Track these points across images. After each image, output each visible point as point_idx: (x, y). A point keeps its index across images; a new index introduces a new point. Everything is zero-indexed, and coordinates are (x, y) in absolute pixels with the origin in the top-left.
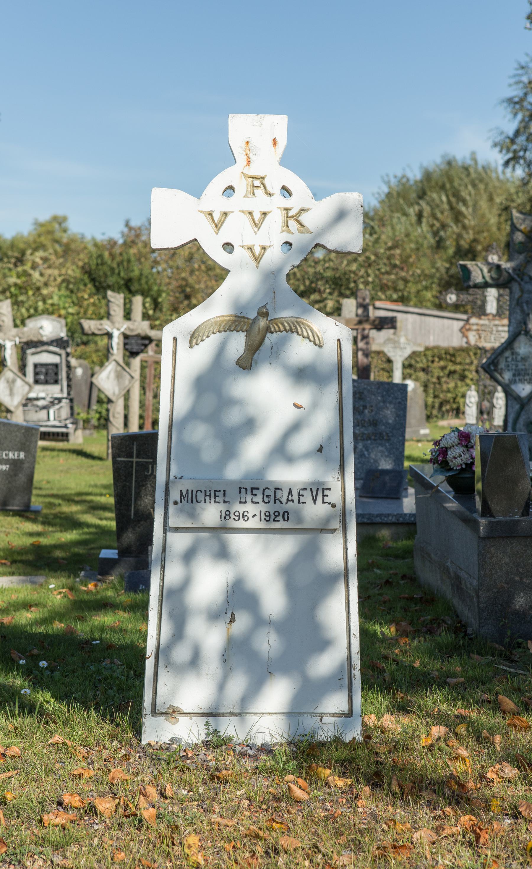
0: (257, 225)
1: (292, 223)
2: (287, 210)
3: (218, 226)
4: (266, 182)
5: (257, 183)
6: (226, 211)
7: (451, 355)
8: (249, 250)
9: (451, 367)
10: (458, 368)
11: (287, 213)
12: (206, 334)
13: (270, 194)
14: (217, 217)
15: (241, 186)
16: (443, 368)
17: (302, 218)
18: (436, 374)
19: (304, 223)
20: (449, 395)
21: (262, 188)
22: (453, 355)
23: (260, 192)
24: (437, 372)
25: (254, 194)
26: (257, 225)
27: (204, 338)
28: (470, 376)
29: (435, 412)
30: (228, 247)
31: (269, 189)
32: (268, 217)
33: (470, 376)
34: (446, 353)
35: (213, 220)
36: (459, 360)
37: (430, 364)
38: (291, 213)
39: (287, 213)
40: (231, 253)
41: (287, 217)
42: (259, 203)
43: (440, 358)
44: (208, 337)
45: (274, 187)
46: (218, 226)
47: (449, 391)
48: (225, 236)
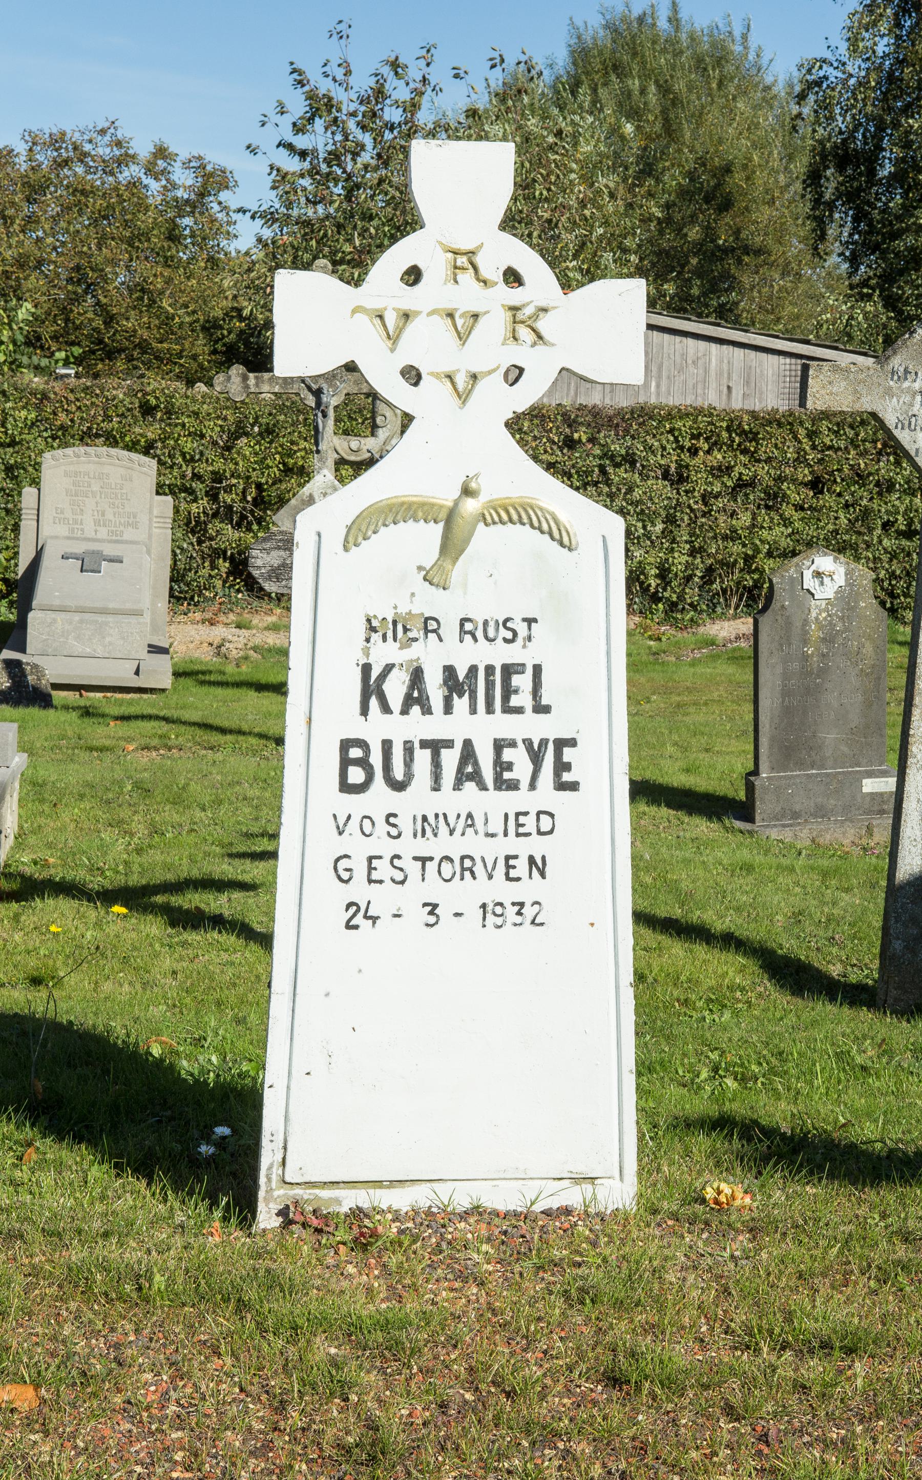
0: (462, 337)
1: (524, 333)
2: (514, 309)
3: (393, 339)
4: (479, 260)
5: (462, 261)
6: (475, 369)
7: (744, 433)
8: (377, 321)
9: (742, 469)
10: (762, 470)
11: (514, 316)
12: (372, 527)
13: (485, 282)
14: (461, 381)
15: (435, 268)
16: (724, 470)
17: (541, 325)
18: (702, 487)
19: (544, 333)
20: (736, 548)
21: (471, 271)
22: (753, 436)
23: (466, 278)
24: (701, 482)
25: (456, 282)
26: (462, 337)
27: (370, 533)
28: (795, 498)
29: (692, 594)
30: (413, 376)
31: (484, 273)
32: (482, 321)
33: (795, 498)
34: (728, 429)
35: (384, 326)
36: (766, 449)
37: (685, 457)
38: (520, 316)
39: (514, 316)
40: (416, 384)
41: (515, 322)
42: (466, 295)
43: (715, 445)
44: (375, 533)
45: (492, 269)
46: (393, 339)
47: (732, 536)
48: (406, 355)
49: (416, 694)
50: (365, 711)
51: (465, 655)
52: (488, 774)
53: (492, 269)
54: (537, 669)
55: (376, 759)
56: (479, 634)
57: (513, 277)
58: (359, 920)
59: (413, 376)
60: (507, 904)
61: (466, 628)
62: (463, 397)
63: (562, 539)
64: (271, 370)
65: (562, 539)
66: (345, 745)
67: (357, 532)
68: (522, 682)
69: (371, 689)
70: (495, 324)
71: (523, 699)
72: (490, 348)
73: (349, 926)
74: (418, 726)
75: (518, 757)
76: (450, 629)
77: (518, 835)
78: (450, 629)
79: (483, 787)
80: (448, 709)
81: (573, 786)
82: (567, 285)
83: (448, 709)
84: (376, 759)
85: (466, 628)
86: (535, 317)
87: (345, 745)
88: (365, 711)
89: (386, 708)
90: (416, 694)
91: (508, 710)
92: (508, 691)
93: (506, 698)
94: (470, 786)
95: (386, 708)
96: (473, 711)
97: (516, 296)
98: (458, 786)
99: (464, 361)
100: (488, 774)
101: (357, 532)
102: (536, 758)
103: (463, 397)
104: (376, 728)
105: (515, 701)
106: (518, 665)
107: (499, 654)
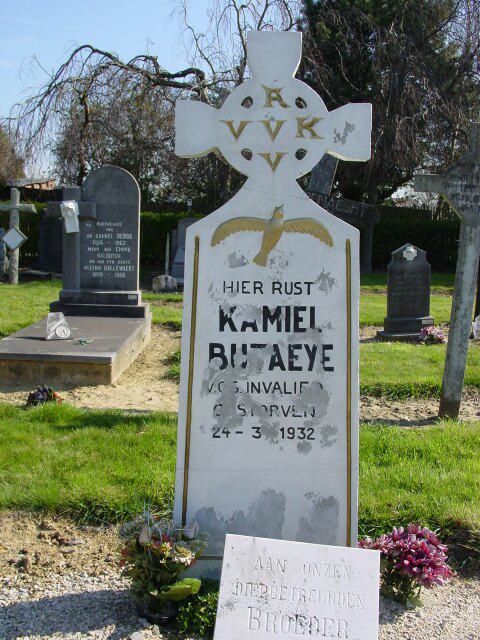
15: (260, 98)
30: (248, 155)
31: (286, 100)
45: (289, 97)
49: (277, 360)
50: (222, 329)
51: (274, 301)
52: (286, 365)
53: (289, 97)
54: (313, 309)
55: (228, 353)
56: (283, 289)
57: (300, 103)
58: (219, 434)
59: (248, 155)
60: (296, 429)
61: (277, 287)
62: (274, 166)
63: (325, 237)
64: (383, 555)
65: (325, 237)
66: (212, 346)
67: (217, 238)
68: (305, 315)
69: (224, 320)
70: (290, 127)
71: (305, 324)
72: (289, 141)
73: (214, 436)
74: (250, 337)
75: (302, 354)
76: (267, 288)
77: (294, 416)
78: (267, 288)
79: (283, 368)
80: (265, 329)
81: (331, 369)
82: (331, 107)
83: (265, 329)
84: (228, 353)
85: (277, 287)
86: (312, 124)
87: (212, 346)
88: (222, 329)
89: (233, 329)
90: (277, 360)
91: (297, 329)
92: (298, 320)
93: (296, 325)
94: (277, 368)
95: (233, 329)
96: (279, 330)
97: (302, 113)
98: (271, 368)
99: (273, 149)
100: (286, 365)
101: (217, 238)
102: (312, 355)
103: (274, 166)
104: (227, 338)
105: (301, 325)
106: (304, 188)
107: (293, 301)
